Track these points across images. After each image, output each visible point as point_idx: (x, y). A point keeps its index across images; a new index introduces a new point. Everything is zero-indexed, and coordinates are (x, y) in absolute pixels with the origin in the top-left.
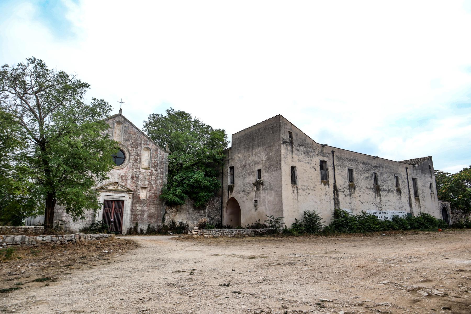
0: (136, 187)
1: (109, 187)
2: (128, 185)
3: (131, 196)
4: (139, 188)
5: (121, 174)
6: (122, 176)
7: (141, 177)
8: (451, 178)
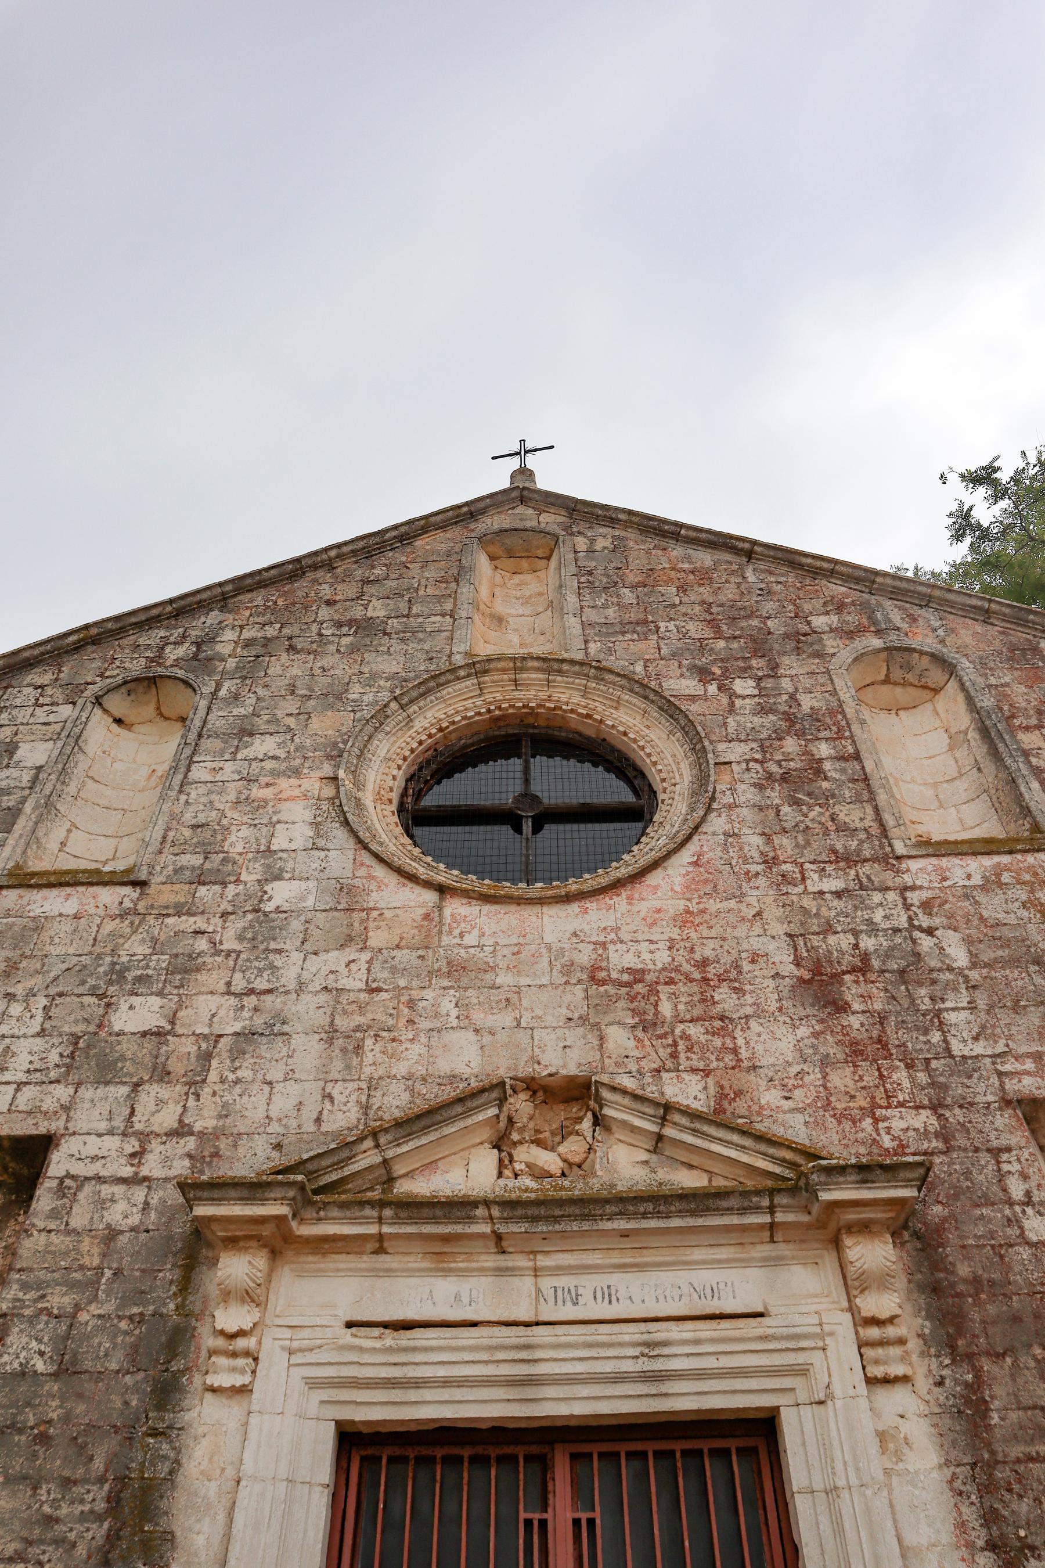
0: (924, 1119)
1: (431, 1166)
2: (771, 1097)
3: (882, 1281)
4: (1003, 1119)
5: (621, 959)
6: (638, 975)
7: (960, 956)
8: (946, 1270)
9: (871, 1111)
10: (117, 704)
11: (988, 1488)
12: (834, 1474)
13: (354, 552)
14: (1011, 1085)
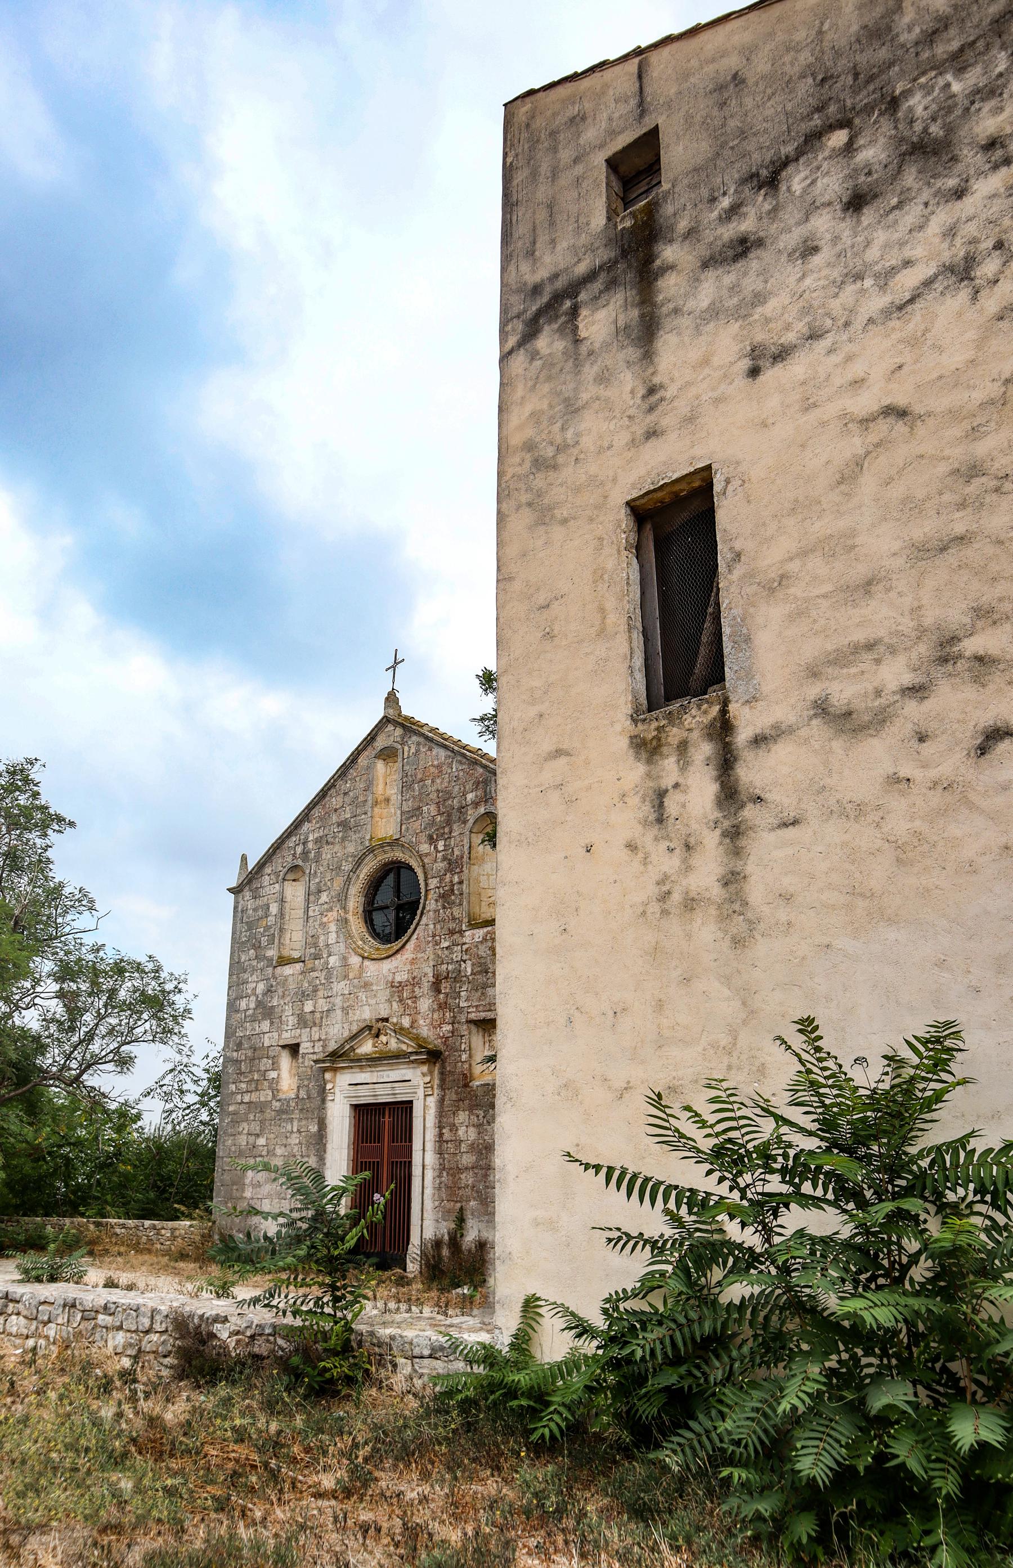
9: (439, 1026)
10: (290, 876)
11: (441, 1116)
12: (941, 377)
13: (339, 776)
14: (470, 1016)
